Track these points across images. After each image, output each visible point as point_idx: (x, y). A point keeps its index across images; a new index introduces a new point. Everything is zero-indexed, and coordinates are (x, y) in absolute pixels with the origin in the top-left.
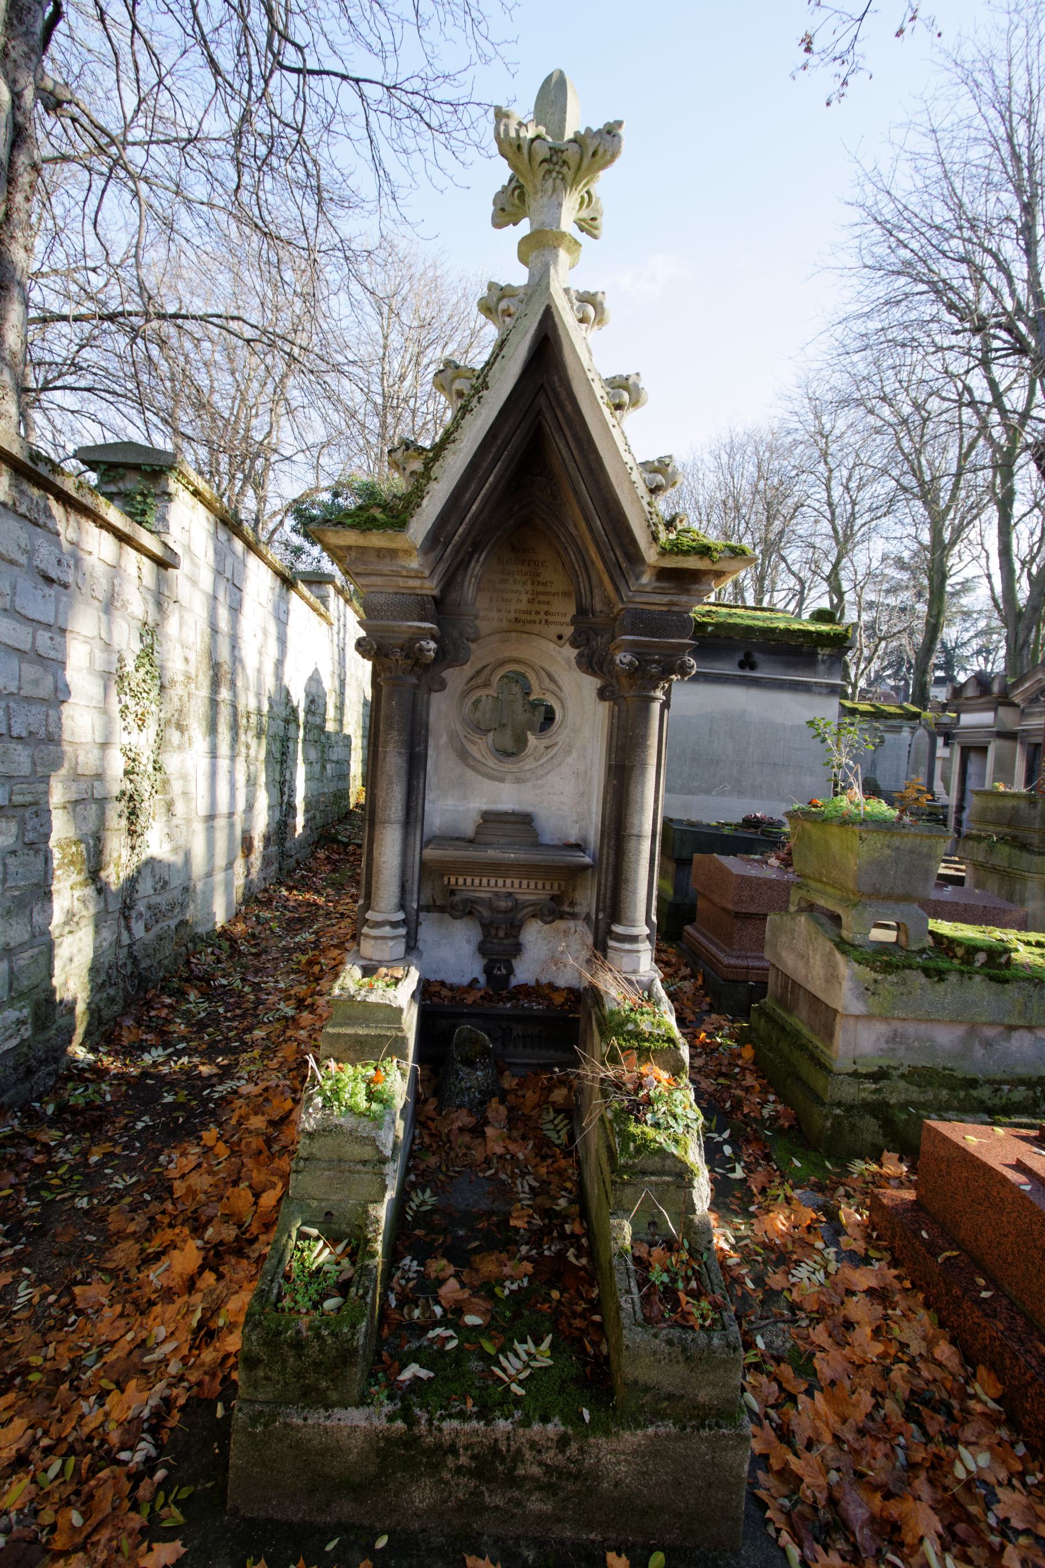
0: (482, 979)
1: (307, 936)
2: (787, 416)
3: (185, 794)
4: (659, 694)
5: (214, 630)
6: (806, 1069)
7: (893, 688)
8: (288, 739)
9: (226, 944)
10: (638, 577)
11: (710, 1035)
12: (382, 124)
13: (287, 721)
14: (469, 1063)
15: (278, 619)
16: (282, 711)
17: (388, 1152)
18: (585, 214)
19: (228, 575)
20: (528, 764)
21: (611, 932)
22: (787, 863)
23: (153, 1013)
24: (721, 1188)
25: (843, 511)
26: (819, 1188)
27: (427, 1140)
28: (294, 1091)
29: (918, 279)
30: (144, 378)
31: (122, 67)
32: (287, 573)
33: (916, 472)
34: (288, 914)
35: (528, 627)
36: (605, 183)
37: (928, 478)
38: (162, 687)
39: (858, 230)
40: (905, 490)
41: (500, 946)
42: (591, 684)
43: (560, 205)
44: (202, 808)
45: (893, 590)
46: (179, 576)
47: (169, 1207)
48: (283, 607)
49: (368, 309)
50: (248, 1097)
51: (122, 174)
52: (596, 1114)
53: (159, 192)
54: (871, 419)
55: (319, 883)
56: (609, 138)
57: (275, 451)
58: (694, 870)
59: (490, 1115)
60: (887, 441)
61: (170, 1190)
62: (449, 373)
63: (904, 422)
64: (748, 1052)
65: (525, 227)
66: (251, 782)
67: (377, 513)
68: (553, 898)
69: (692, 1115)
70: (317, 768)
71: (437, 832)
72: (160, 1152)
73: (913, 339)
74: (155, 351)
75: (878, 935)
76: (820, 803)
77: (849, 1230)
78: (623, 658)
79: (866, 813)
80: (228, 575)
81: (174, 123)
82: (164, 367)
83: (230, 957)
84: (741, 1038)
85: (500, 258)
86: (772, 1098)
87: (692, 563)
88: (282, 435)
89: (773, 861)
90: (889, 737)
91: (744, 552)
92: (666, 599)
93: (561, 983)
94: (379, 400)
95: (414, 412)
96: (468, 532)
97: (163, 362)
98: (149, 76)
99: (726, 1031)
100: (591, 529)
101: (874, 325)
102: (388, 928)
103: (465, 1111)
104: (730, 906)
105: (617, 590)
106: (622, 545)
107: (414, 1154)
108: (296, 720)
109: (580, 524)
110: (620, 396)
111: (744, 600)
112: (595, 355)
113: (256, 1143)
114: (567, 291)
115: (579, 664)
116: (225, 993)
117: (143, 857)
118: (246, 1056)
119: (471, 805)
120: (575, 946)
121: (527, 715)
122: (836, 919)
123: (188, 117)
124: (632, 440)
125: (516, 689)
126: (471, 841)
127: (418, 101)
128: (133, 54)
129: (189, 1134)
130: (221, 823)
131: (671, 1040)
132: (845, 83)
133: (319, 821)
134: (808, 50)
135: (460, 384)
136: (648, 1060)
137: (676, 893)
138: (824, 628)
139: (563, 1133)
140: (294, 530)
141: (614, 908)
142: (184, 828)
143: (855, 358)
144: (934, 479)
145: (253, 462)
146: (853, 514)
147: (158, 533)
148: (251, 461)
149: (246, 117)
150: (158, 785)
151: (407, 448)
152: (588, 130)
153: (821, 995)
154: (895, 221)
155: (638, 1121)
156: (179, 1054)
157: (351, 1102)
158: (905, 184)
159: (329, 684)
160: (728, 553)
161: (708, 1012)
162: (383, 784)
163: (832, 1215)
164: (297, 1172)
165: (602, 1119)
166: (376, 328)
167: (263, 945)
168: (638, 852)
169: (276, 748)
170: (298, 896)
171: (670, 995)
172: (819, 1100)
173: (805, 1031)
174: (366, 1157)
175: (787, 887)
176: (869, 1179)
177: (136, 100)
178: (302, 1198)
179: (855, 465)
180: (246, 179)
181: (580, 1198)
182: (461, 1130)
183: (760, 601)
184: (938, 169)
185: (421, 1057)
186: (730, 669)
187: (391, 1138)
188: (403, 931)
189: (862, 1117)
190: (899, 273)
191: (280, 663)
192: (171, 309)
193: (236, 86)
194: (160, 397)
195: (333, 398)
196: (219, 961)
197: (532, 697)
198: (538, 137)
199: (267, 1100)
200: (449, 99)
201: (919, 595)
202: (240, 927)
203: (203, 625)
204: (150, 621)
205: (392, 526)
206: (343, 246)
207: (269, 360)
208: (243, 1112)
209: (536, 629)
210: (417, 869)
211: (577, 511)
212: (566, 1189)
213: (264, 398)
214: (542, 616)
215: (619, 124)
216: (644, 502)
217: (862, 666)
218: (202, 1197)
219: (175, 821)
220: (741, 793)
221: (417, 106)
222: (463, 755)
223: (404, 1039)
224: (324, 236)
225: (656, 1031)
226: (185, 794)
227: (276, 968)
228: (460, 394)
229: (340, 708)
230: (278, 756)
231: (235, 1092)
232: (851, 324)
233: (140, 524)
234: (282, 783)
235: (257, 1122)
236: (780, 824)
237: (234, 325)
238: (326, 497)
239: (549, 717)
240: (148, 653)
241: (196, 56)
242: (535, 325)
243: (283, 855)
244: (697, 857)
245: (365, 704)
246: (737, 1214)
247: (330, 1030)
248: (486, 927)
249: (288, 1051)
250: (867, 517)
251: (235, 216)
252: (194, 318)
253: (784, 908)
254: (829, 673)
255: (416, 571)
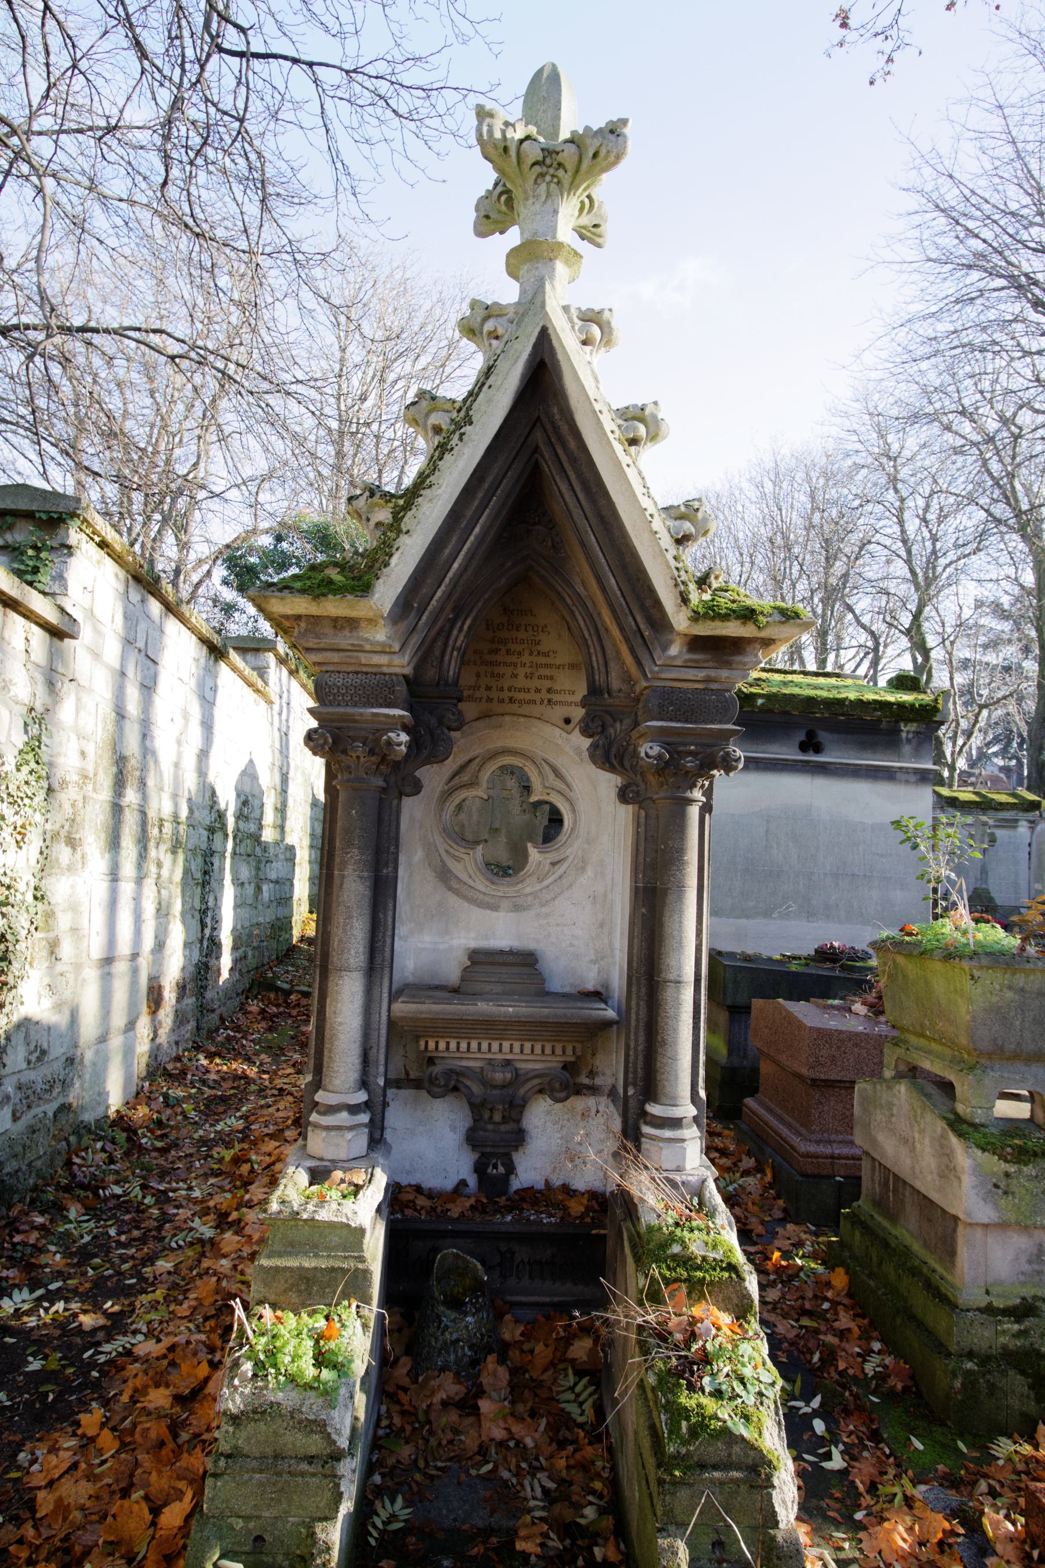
0: (472, 1181)
1: (232, 1122)
2: (844, 435)
3: (74, 930)
4: (697, 794)
5: (121, 715)
6: (920, 1301)
7: (1002, 769)
8: (212, 853)
9: (121, 1136)
10: (665, 648)
11: (786, 1255)
12: (340, 112)
13: (211, 830)
14: (456, 1304)
15: (203, 698)
16: (205, 817)
17: (343, 1443)
18: (586, 220)
19: (141, 644)
20: (530, 887)
21: (645, 1113)
22: (877, 1009)
23: (17, 1238)
24: (814, 1485)
25: (921, 552)
26: (951, 1482)
27: (397, 1420)
28: (212, 1350)
29: (992, 273)
30: (41, 402)
31: (29, 50)
32: (216, 639)
33: (1010, 498)
34: (208, 1092)
35: (526, 709)
36: (608, 187)
37: (1025, 507)
38: (50, 790)
39: (917, 219)
40: (998, 521)
41: (495, 1137)
42: (608, 782)
43: (556, 212)
44: (96, 949)
45: (993, 644)
46: (77, 649)
47: (29, 1532)
48: (209, 683)
49: (322, 318)
50: (146, 1360)
51: (25, 168)
52: (633, 1378)
53: (68, 187)
54: (948, 436)
55: (250, 1047)
56: (612, 137)
57: (203, 487)
58: (753, 1022)
59: (485, 1380)
60: (970, 461)
61: (31, 1506)
62: (423, 407)
63: (990, 440)
64: (840, 1279)
65: (513, 237)
66: (162, 912)
67: (334, 574)
68: (565, 1067)
69: (766, 1378)
70: (250, 890)
71: (411, 979)
72: (19, 1447)
73: (995, 343)
74: (55, 370)
75: (1005, 1109)
76: (915, 928)
77: (999, 1548)
78: (649, 749)
79: (977, 943)
80: (141, 644)
81: (90, 111)
82: (66, 389)
83: (127, 1154)
84: (830, 1258)
85: (486, 272)
86: (876, 1346)
87: (733, 629)
88: (212, 468)
89: (859, 1008)
90: (999, 833)
91: (797, 615)
92: (701, 674)
93: (581, 1183)
94: (334, 425)
95: (377, 437)
96: (448, 596)
97: (65, 381)
98: (61, 60)
99: (808, 1249)
100: (604, 590)
101: (944, 326)
102: (344, 1114)
103: (449, 1376)
104: (804, 1071)
105: (639, 664)
106: (643, 608)
107: (379, 1440)
108: (223, 827)
109: (589, 580)
110: (635, 429)
111: (802, 662)
112: (600, 383)
113: (157, 1429)
114: (566, 309)
115: (593, 758)
116: (118, 1207)
117: (15, 1018)
118: (144, 1299)
119: (456, 942)
120: (598, 1134)
121: (527, 817)
122: (947, 1088)
123: (105, 102)
124: (649, 483)
125: (511, 783)
126: (456, 991)
127: (383, 87)
128: (44, 37)
129: (61, 1419)
130: (121, 967)
131: (732, 1268)
132: (890, 60)
133: (251, 962)
134: (844, 25)
135: (439, 420)
136: (702, 1296)
137: (730, 1052)
138: (907, 697)
139: (588, 1406)
140: (225, 582)
141: (648, 1079)
142: (71, 977)
143: (924, 365)
144: (1033, 508)
145: (174, 501)
146: (934, 552)
147: (53, 595)
148: (170, 499)
149: (177, 104)
150: (39, 920)
151: (372, 495)
152: (587, 129)
153: (934, 1196)
154: (961, 208)
155: (691, 1388)
156: (52, 1297)
157: (293, 1369)
158: (971, 166)
159: (267, 780)
160: (777, 617)
161: (782, 1221)
162: (339, 918)
163: (973, 1524)
164: (215, 1475)
165: (641, 1385)
166: (330, 338)
167: (173, 1136)
168: (678, 1004)
169: (196, 865)
170: (223, 1066)
171: (728, 1199)
172: (941, 1348)
173: (916, 1247)
174: (313, 1450)
175: (880, 1042)
176: (1021, 1467)
177: (45, 85)
178: (222, 1517)
179: (933, 493)
180: (175, 172)
181: (614, 1505)
182: (445, 1404)
183: (822, 662)
184: (1009, 149)
185: (388, 1299)
186: (790, 753)
187: (348, 1421)
188: (364, 1118)
189: (1004, 1374)
190: (970, 267)
191: (204, 754)
192: (78, 322)
193: (167, 72)
194: (60, 425)
195: (274, 421)
196: (111, 1160)
197: (534, 798)
198: (528, 138)
199: (173, 1364)
200: (420, 84)
201: (1026, 650)
202: (142, 1111)
203: (106, 709)
204: (39, 707)
205: (352, 590)
206: (293, 248)
207: (198, 379)
208: (138, 1382)
209: (537, 710)
210: (384, 1032)
211: (586, 568)
212: (593, 1492)
213: (189, 424)
214: (544, 695)
215: (624, 122)
216: (669, 556)
217: (960, 741)
218: (77, 1515)
219: (60, 967)
220: (810, 915)
221: (382, 92)
222: (444, 876)
223: (366, 1273)
224: (269, 235)
225: (711, 1255)
226: (74, 930)
227: (189, 1169)
228: (437, 430)
229: (282, 810)
230: (198, 875)
231: (128, 1353)
232: (916, 326)
233: (30, 584)
234: (204, 912)
235: (159, 1398)
236: (866, 957)
237: (155, 339)
238: (266, 541)
239: (556, 820)
240: (34, 747)
241: (119, 37)
242: (529, 349)
243: (203, 1009)
244: (757, 1003)
245: (315, 803)
246: (837, 1525)
247: (264, 1262)
248: (477, 1108)
249: (203, 1290)
250: (951, 556)
251: (160, 215)
252: (107, 331)
253: (876, 1073)
254: (917, 754)
255: (383, 644)
